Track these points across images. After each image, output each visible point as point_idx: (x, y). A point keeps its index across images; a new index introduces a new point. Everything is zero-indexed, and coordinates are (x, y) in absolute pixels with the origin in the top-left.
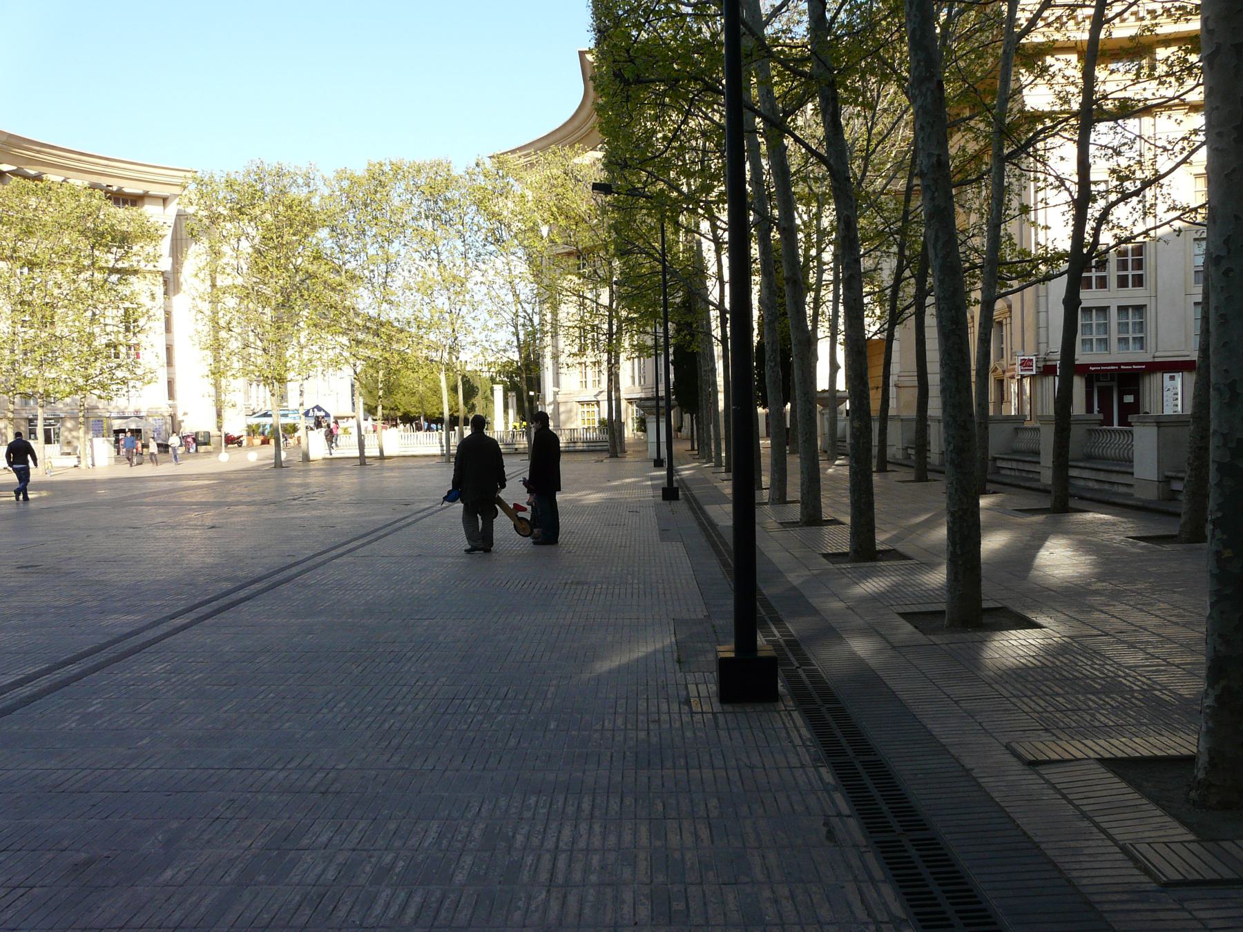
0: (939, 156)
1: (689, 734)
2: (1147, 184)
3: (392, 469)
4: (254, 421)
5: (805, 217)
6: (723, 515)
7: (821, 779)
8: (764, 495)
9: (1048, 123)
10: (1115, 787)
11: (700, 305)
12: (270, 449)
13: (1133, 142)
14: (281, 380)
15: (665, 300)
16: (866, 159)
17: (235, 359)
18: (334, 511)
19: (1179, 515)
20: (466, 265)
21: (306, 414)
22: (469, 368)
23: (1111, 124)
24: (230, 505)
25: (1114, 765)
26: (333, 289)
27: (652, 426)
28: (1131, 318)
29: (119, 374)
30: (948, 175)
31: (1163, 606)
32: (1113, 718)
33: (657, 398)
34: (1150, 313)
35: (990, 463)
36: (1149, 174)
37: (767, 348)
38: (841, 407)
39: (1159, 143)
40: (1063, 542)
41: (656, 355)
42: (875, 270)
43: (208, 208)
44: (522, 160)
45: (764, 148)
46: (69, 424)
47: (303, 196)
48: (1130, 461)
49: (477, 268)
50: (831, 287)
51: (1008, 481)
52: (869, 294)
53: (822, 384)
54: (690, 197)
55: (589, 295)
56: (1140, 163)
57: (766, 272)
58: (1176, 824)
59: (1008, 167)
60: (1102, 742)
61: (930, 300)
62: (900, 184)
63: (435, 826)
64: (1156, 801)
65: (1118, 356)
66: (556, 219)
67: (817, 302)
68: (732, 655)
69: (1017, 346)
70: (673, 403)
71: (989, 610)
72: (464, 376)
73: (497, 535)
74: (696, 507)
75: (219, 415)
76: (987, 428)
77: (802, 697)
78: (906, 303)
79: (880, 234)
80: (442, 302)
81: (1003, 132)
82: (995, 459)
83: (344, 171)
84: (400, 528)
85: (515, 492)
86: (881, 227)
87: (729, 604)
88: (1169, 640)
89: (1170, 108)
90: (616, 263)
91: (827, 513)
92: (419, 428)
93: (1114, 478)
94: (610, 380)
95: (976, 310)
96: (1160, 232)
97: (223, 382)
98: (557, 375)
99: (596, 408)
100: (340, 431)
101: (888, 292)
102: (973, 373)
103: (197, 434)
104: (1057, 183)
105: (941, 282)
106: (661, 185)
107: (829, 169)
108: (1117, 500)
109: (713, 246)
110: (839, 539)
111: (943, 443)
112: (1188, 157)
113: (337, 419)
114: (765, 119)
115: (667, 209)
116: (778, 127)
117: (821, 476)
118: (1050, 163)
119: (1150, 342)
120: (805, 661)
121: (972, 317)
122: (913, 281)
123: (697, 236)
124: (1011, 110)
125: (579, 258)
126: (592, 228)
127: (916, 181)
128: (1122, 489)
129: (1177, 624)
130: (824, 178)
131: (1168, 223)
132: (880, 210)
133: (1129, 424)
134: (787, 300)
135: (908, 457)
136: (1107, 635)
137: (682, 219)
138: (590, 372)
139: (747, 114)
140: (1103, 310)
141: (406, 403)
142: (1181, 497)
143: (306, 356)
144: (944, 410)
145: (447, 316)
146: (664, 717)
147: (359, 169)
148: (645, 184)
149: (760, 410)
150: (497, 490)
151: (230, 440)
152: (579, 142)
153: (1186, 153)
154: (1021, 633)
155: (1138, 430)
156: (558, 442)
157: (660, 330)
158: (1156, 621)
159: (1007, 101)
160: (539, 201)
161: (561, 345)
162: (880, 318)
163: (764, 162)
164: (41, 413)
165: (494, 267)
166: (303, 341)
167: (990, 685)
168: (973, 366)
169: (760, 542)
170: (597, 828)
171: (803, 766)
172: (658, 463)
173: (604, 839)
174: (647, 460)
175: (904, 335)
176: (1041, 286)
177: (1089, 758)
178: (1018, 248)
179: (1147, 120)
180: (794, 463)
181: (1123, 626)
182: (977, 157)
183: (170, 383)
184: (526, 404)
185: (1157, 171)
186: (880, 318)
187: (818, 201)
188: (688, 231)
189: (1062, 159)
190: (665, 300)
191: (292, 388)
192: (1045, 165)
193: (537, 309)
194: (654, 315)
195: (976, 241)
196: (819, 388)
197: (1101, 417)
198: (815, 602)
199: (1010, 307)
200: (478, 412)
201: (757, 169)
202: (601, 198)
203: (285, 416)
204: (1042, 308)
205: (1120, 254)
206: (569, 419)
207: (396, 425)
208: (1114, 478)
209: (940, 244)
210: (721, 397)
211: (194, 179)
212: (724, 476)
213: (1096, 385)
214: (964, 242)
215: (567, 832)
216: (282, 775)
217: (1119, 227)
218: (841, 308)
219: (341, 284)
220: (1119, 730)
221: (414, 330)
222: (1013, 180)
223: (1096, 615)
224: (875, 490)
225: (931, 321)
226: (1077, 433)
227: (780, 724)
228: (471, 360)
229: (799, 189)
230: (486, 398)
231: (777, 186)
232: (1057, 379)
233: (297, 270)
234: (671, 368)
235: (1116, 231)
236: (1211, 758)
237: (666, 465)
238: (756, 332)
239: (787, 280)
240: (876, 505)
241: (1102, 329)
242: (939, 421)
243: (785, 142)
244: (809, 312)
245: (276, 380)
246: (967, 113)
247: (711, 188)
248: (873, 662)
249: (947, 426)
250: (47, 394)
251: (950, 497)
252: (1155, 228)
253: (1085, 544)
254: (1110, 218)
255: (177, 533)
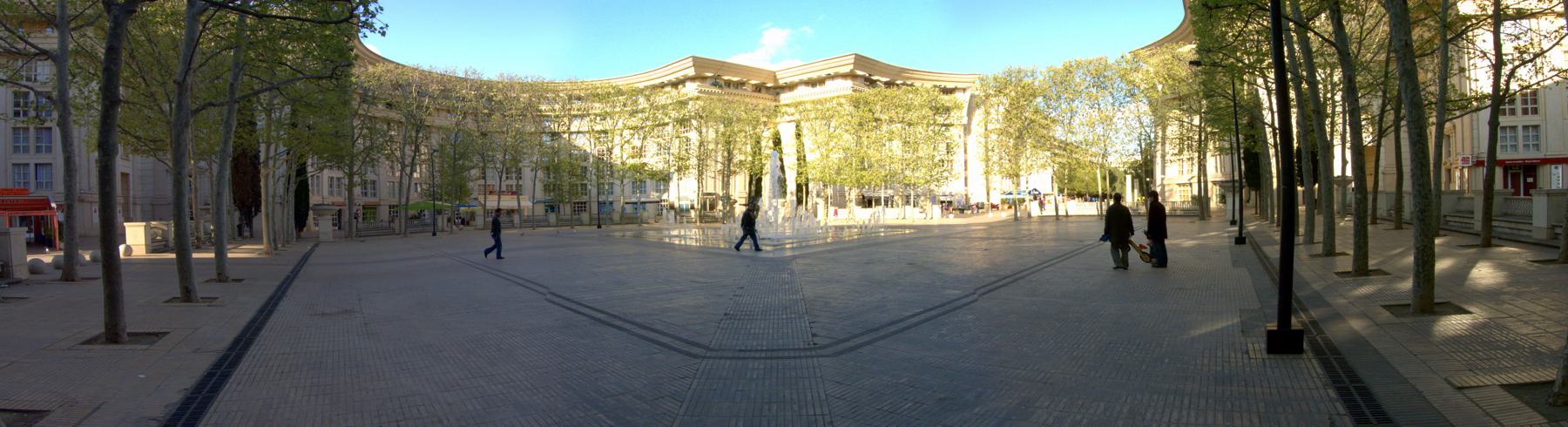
0: (1406, 40)
1: (1248, 369)
2: (1536, 56)
3: (1072, 222)
4: (1004, 197)
5: (1323, 76)
6: (1274, 252)
7: (1328, 394)
8: (1300, 239)
9: (1474, 21)
10: (1509, 398)
11: (1259, 125)
12: (1012, 211)
13: (1527, 32)
14: (1018, 176)
15: (1236, 121)
16: (1360, 43)
17: (995, 165)
18: (1044, 244)
19: (1559, 248)
20: (1114, 109)
21: (1029, 193)
22: (1113, 166)
23: (1513, 22)
24: (993, 239)
25: (1509, 388)
26: (1044, 128)
27: (1229, 200)
28: (1531, 133)
29: (945, 174)
30: (1412, 51)
31: (1546, 300)
32: (1511, 363)
33: (1234, 181)
34: (1542, 129)
35: (1442, 219)
36: (1537, 50)
37: (1303, 151)
38: (1349, 186)
39: (1542, 33)
40: (1487, 264)
41: (1232, 153)
42: (1368, 105)
43: (985, 91)
44: (1148, 53)
45: (1295, 39)
46: (922, 198)
47: (1030, 82)
48: (1531, 217)
49: (1119, 110)
50: (1341, 115)
51: (1454, 229)
52: (1365, 119)
53: (1337, 172)
54: (1250, 66)
55: (1186, 120)
56: (1531, 44)
57: (1300, 106)
58: (1538, 415)
59: (1450, 46)
60: (1503, 376)
61: (1403, 123)
62: (1383, 57)
63: (1102, 405)
64: (1527, 403)
65: (1523, 154)
66: (1166, 81)
67: (1333, 124)
68: (1276, 328)
69: (1459, 149)
70: (1244, 184)
71: (1371, 271)
72: (1110, 171)
73: (1130, 261)
74: (1257, 248)
75: (988, 194)
76: (1440, 198)
77: (1318, 351)
78: (1388, 125)
79: (1370, 85)
80: (1099, 130)
81: (1446, 26)
82: (1445, 216)
83: (1051, 67)
84: (1077, 254)
85: (1139, 237)
86: (1371, 81)
87: (1275, 301)
88: (1549, 319)
89: (1546, 14)
90: (1204, 102)
91: (1338, 249)
92: (1086, 200)
93: (1520, 226)
94: (1200, 169)
95: (1433, 129)
96: (1546, 83)
97: (990, 177)
98: (1163, 167)
99: (1189, 188)
100: (1046, 202)
101: (1377, 118)
102: (1432, 166)
103: (978, 203)
104: (1482, 55)
105: (1410, 112)
106: (1232, 60)
107: (1337, 48)
108: (1523, 240)
109: (1265, 92)
110: (1346, 263)
111: (1412, 207)
112: (1559, 41)
113: (1044, 195)
114: (1295, 23)
115: (1236, 73)
116: (1303, 27)
117: (1336, 227)
118: (1476, 43)
119: (1543, 147)
120: (1321, 332)
121: (1431, 133)
122: (1392, 112)
123: (1255, 87)
124: (1450, 14)
125: (1180, 100)
126: (1189, 84)
127: (1392, 55)
128: (1526, 233)
129: (1553, 310)
130: (1334, 54)
131: (1551, 78)
132: (1370, 71)
133: (1530, 195)
134: (1314, 123)
135: (1390, 215)
136: (1512, 317)
137: (1245, 77)
138: (1187, 165)
139: (1284, 21)
140: (1514, 128)
141: (1079, 186)
142: (1561, 237)
143: (1029, 163)
144: (1413, 186)
145: (1102, 138)
146: (1233, 360)
147: (1059, 66)
148: (1222, 60)
149: (1299, 188)
150: (1129, 236)
151: (993, 206)
152: (1181, 40)
153: (1558, 39)
154: (1458, 317)
155: (1535, 198)
156: (1164, 209)
157: (1234, 139)
158: (1541, 308)
159: (1447, 9)
160: (1157, 73)
161: (1167, 149)
162: (1372, 133)
163: (1296, 46)
164: (912, 193)
165: (1129, 109)
166: (1028, 156)
167: (1437, 346)
168: (1432, 161)
169: (1296, 266)
170: (1192, 413)
171: (1317, 388)
172: (1233, 223)
173: (1196, 419)
174: (1226, 221)
175: (1388, 143)
176: (1474, 114)
177: (1495, 385)
178: (1459, 92)
179: (1533, 21)
180: (1319, 220)
181: (1522, 312)
182: (1430, 41)
183: (966, 179)
184: (1145, 186)
185: (1542, 49)
186: (1372, 133)
187: (1330, 67)
188: (1249, 84)
189: (1484, 41)
190: (1236, 121)
191: (1023, 180)
192: (1474, 44)
193: (1153, 130)
194: (1229, 130)
195: (1432, 89)
196: (1336, 175)
197: (1513, 190)
198: (1328, 299)
199: (1454, 126)
200: (1118, 191)
201: (1291, 50)
202: (1195, 68)
203: (1019, 194)
204: (1475, 127)
205: (1522, 95)
206: (1171, 195)
207: (1074, 199)
208: (1520, 226)
209: (1408, 91)
210: (1275, 180)
211: (979, 78)
212: (1275, 229)
213: (1510, 171)
214: (1424, 89)
215: (1175, 415)
216: (1024, 372)
217: (1522, 80)
218: (1348, 128)
219: (1047, 125)
220: (1514, 369)
221: (1084, 147)
222: (1454, 53)
223: (1506, 306)
224: (1369, 235)
225: (1404, 134)
226: (1497, 201)
227: (1304, 365)
228: (1115, 162)
229: (1318, 60)
230: (1122, 183)
231: (1305, 59)
232: (1485, 169)
233: (1026, 118)
234: (1242, 162)
235: (1520, 82)
236: (1563, 381)
237: (1238, 223)
238: (1295, 141)
239: (1314, 111)
240: (1370, 244)
241: (1513, 139)
242: (1410, 194)
243: (1309, 35)
244: (1328, 130)
245: (1015, 176)
246: (1423, 16)
247: (1264, 61)
248: (1364, 333)
249: (1415, 197)
250: (914, 185)
251: (1416, 239)
252: (1544, 81)
253: (1500, 265)
254: (1516, 74)
255: (971, 252)
